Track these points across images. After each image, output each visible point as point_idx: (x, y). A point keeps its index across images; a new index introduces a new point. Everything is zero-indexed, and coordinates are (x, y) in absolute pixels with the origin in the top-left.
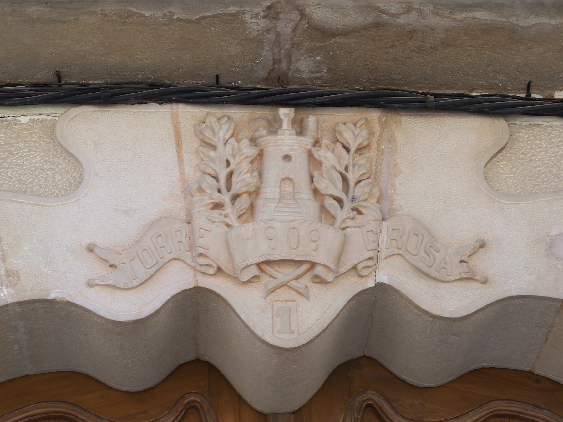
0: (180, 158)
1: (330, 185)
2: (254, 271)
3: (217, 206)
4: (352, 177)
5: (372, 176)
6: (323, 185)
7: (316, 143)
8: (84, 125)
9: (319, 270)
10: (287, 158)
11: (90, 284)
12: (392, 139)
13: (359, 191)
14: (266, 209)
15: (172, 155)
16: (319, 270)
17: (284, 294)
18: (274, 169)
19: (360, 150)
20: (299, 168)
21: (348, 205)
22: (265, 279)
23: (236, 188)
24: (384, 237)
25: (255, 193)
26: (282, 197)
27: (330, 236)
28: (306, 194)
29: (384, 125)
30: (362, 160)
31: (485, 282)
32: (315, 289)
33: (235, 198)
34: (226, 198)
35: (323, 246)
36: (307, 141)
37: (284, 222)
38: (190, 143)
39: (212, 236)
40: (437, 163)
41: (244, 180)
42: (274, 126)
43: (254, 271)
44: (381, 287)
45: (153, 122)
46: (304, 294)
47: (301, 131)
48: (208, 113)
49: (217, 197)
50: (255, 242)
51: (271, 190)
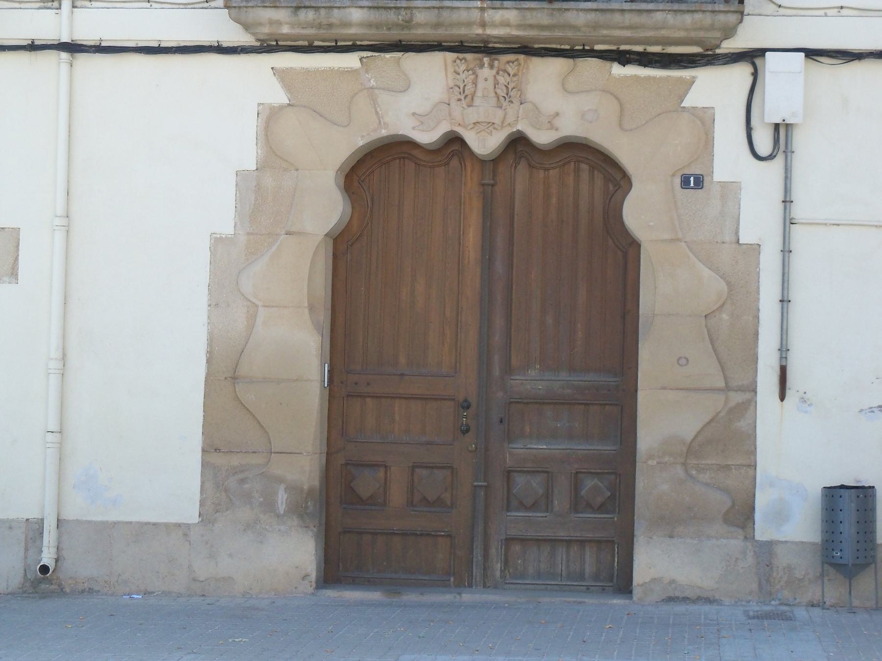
0: (446, 76)
1: (502, 92)
2: (472, 126)
3: (459, 100)
4: (510, 87)
5: (519, 88)
6: (499, 91)
7: (498, 73)
8: (412, 61)
9: (495, 126)
10: (486, 80)
11: (414, 128)
12: (528, 68)
13: (512, 94)
14: (477, 101)
15: (443, 73)
16: (495, 126)
17: (483, 133)
18: (481, 84)
19: (514, 75)
20: (490, 83)
21: (508, 100)
22: (476, 128)
23: (467, 92)
24: (521, 111)
25: (473, 95)
26: (483, 96)
27: (500, 113)
28: (493, 94)
29: (525, 61)
30: (515, 79)
31: (557, 130)
32: (494, 131)
33: (465, 98)
34: (462, 97)
35: (497, 116)
36: (494, 72)
37: (484, 108)
38: (451, 70)
39: (457, 110)
40: (544, 76)
41: (469, 89)
42: (482, 66)
43: (472, 126)
44: (519, 132)
45: (437, 58)
46: (491, 133)
47: (491, 66)
48: (458, 58)
49: (459, 96)
50: (473, 115)
51: (479, 93)
